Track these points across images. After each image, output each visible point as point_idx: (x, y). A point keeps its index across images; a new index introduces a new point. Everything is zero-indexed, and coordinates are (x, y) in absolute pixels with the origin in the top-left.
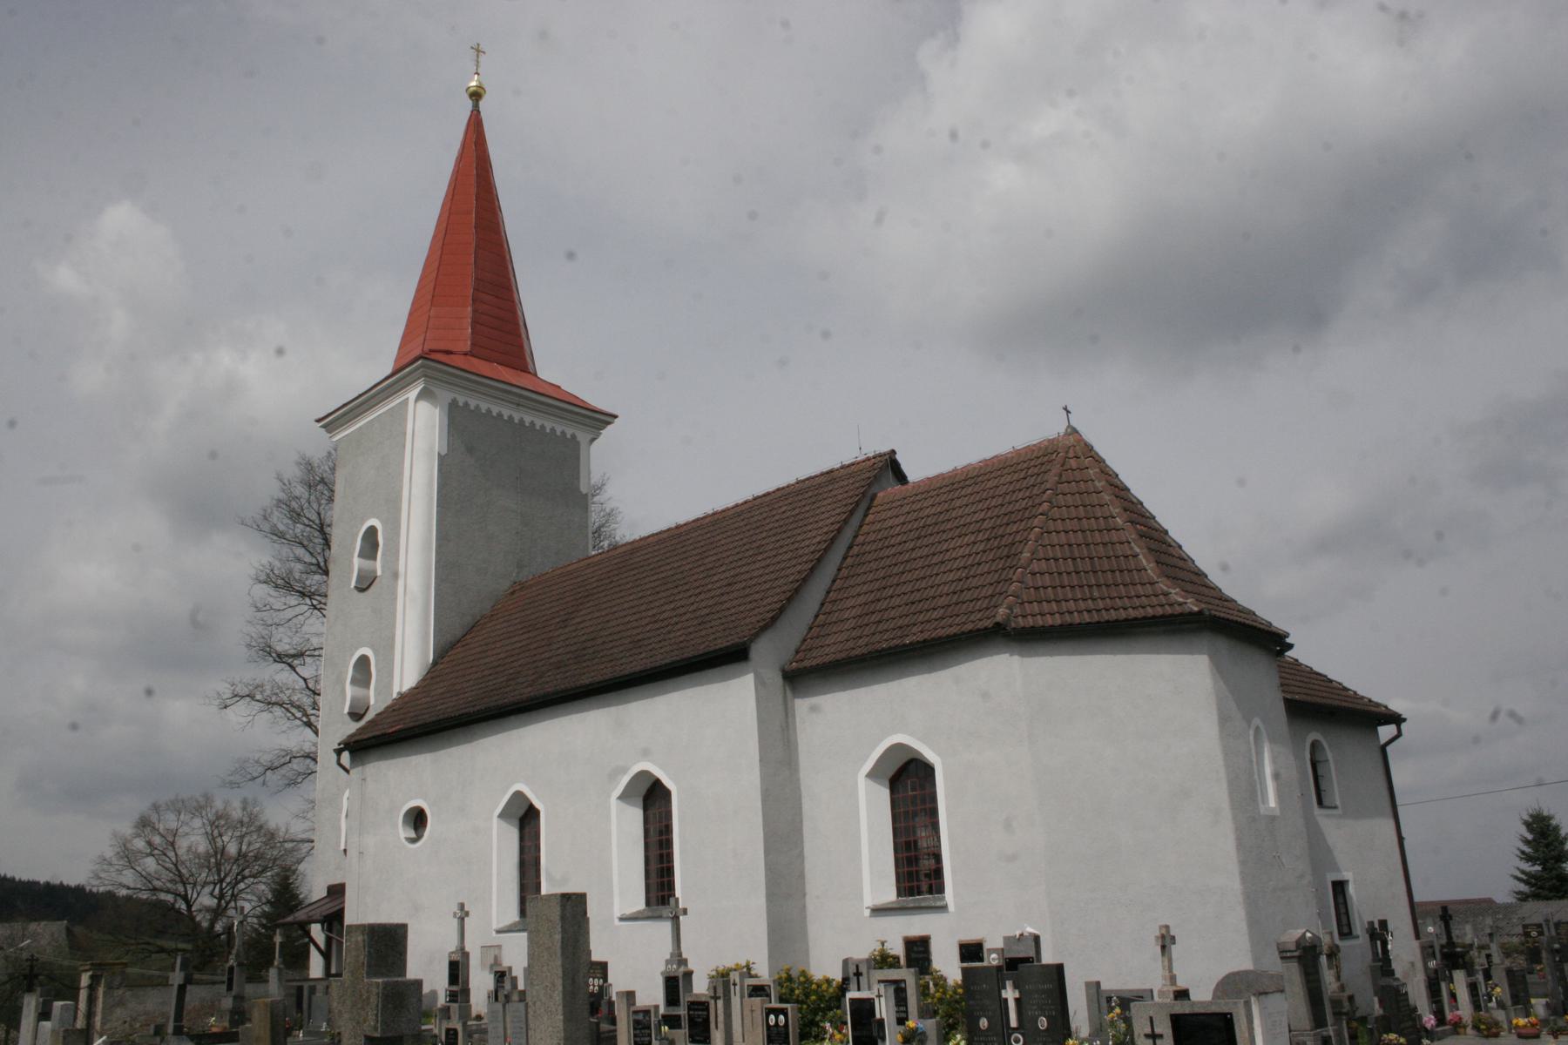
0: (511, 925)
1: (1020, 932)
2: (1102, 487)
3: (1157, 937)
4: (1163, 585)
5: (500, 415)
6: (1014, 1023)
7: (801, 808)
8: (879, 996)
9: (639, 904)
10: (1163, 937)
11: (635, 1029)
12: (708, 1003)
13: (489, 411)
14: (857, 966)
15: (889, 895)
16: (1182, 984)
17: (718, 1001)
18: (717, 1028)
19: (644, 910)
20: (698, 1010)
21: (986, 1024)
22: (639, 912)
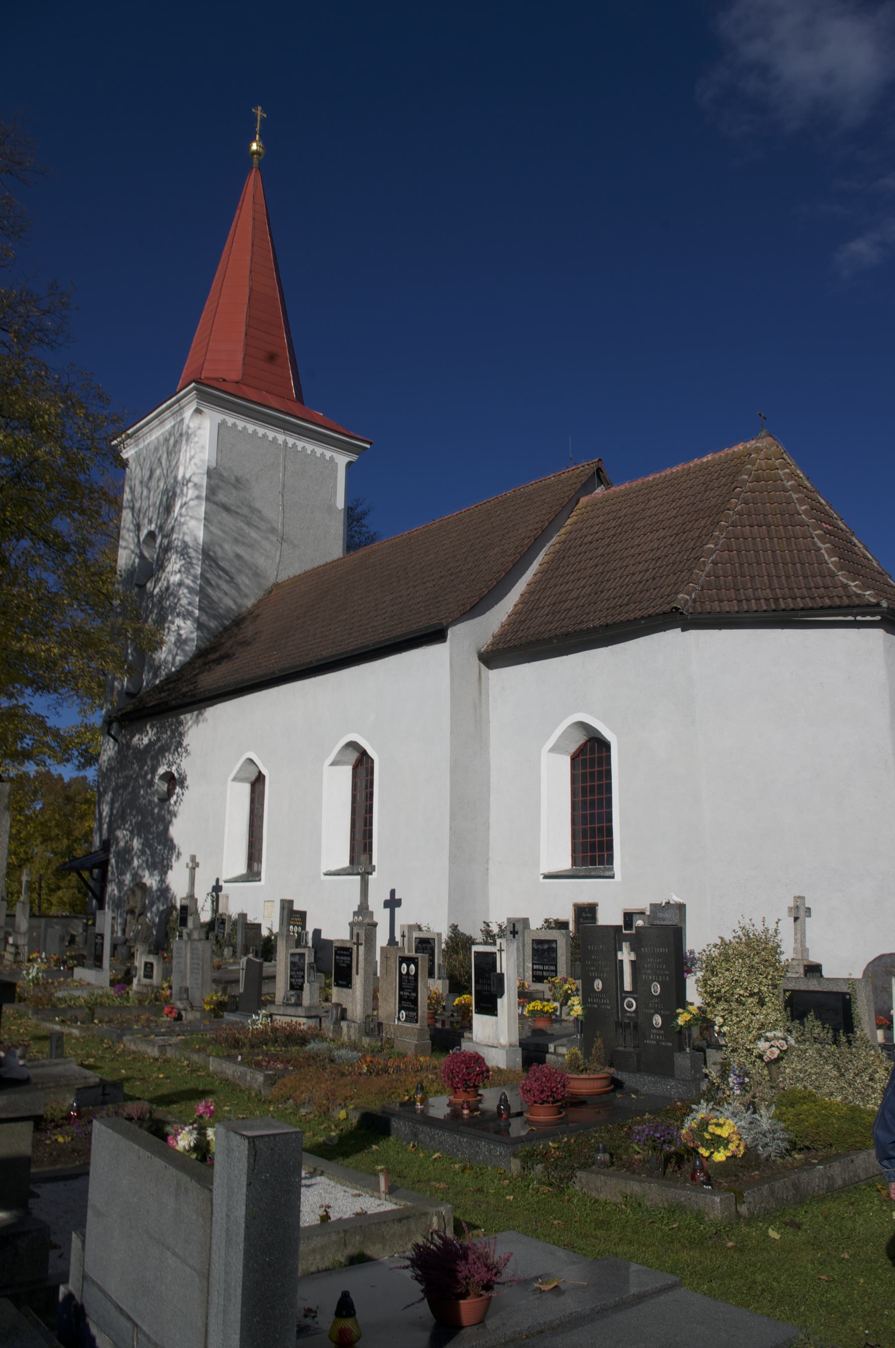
0: (233, 879)
1: (667, 901)
2: (791, 486)
3: (790, 909)
4: (842, 577)
5: (265, 436)
6: (628, 987)
7: (489, 780)
8: (501, 950)
9: (344, 862)
10: (797, 907)
11: (291, 970)
12: (352, 949)
13: (265, 436)
14: (514, 925)
15: (565, 863)
16: (814, 958)
17: (360, 947)
18: (357, 974)
19: (347, 868)
20: (343, 955)
21: (600, 986)
22: (343, 869)
